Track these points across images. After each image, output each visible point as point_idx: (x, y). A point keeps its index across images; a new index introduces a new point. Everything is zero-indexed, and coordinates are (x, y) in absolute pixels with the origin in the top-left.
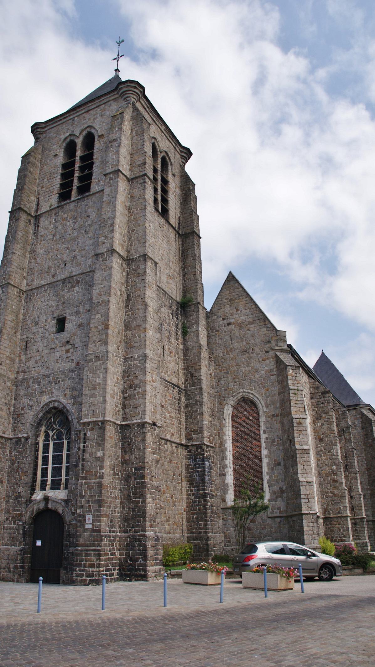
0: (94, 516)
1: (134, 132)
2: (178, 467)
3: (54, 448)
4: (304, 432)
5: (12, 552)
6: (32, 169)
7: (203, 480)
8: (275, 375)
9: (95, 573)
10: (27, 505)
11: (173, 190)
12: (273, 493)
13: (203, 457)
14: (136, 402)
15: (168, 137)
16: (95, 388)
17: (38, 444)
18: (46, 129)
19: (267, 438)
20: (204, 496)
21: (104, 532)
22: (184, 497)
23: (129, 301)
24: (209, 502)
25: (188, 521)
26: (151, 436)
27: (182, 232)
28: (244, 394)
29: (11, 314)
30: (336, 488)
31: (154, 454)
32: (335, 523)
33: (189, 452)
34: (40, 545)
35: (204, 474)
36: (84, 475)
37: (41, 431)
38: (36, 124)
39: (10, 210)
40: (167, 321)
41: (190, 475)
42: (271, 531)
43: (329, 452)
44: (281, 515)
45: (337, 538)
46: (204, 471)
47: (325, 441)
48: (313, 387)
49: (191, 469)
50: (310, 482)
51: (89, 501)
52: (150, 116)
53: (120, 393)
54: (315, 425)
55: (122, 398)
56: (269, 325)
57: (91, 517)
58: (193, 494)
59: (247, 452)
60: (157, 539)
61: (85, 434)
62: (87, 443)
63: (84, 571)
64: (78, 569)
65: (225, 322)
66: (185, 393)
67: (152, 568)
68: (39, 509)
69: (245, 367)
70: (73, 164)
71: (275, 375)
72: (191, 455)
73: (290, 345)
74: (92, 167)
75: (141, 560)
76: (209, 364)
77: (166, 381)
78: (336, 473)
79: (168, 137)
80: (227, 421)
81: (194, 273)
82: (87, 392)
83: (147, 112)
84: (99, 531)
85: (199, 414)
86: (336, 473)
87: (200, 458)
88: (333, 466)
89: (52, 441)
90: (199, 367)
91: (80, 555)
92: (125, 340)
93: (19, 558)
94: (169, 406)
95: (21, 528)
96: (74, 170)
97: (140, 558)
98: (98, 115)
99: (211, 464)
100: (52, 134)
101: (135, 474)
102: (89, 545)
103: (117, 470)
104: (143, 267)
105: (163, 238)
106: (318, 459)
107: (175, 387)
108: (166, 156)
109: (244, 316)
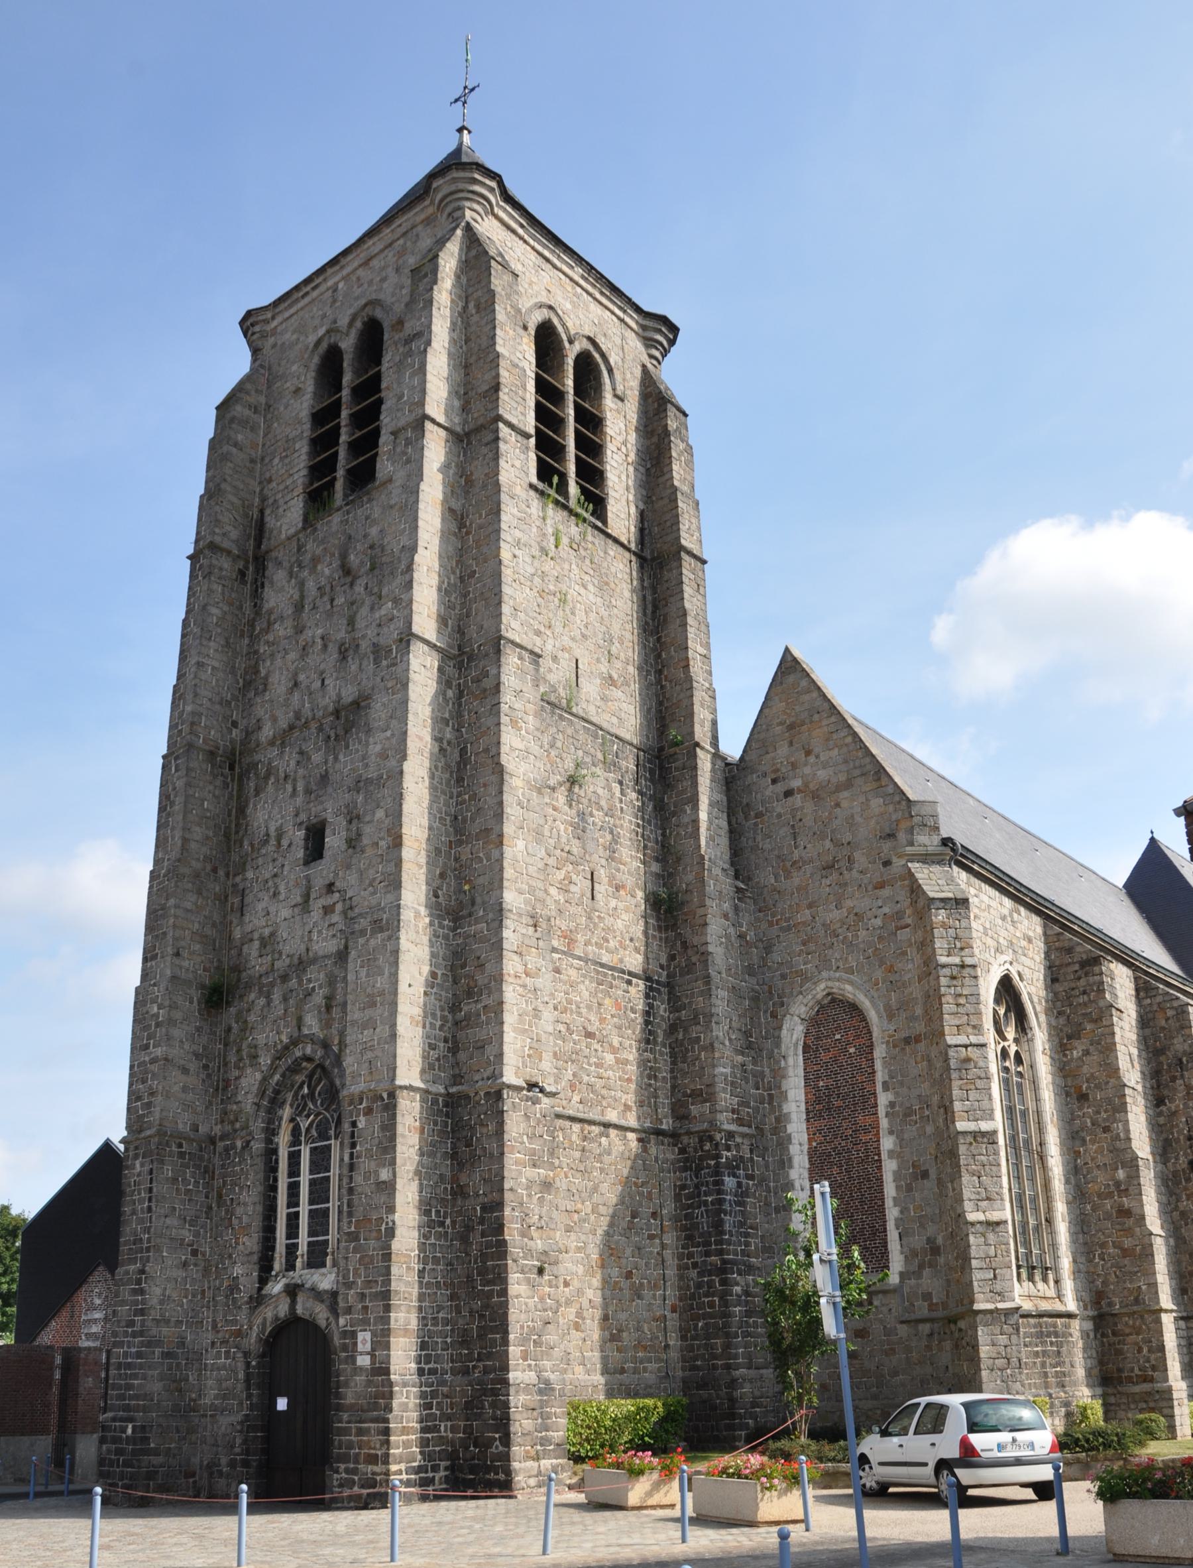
0: (374, 1335)
1: (471, 305)
2: (650, 1193)
3: (312, 1162)
4: (979, 1083)
5: (223, 1428)
6: (240, 437)
7: (718, 1225)
8: (907, 926)
9: (378, 1478)
10: (253, 1310)
11: (620, 439)
12: (910, 1255)
13: (718, 1165)
14: (481, 1034)
15: (598, 296)
16: (373, 1004)
17: (275, 1151)
18: (275, 323)
19: (892, 1105)
20: (723, 1270)
21: (400, 1375)
22: (671, 1272)
23: (465, 766)
24: (737, 1284)
25: (683, 1338)
26: (521, 1119)
27: (652, 552)
28: (830, 984)
29: (199, 825)
30: (1128, 1232)
31: (534, 1166)
32: (1127, 1331)
33: (682, 1151)
34: (285, 1408)
35: (720, 1211)
36: (353, 1229)
37: (281, 1118)
38: (249, 314)
39: (191, 551)
40: (603, 803)
41: (686, 1215)
42: (907, 1358)
43: (1106, 1129)
44: (934, 1315)
45: (1132, 1370)
46: (720, 1202)
47: (1095, 1099)
48: (1057, 949)
49: (688, 1197)
50: (998, 1224)
51: (363, 1296)
52: (533, 248)
53: (442, 1010)
54: (1064, 1055)
55: (449, 1025)
56: (890, 789)
57: (367, 1336)
58: (695, 1265)
59: (843, 1144)
60: (545, 1388)
61: (354, 1124)
62: (358, 1148)
63: (355, 1471)
64: (342, 1466)
65: (780, 788)
66: (669, 993)
67: (523, 1468)
68: (277, 1318)
69: (832, 911)
70: (333, 410)
71: (907, 926)
72: (686, 1160)
73: (950, 839)
74: (379, 412)
75: (498, 1443)
76: (736, 909)
77: (603, 965)
78: (1127, 1190)
79: (598, 296)
80: (791, 1061)
81: (682, 664)
82: (356, 1016)
83: (521, 238)
84: (387, 1372)
85: (704, 1048)
86: (1127, 1190)
87: (709, 1166)
88: (1117, 1169)
89: (306, 1144)
90: (701, 921)
91: (346, 1432)
92: (455, 870)
93: (238, 1441)
94: (615, 1031)
95: (241, 1365)
96: (338, 426)
97: (495, 1439)
98: (390, 269)
99: (744, 1181)
100: (287, 336)
101: (482, 1221)
102: (366, 1407)
103: (438, 1212)
104: (493, 671)
105: (587, 578)
106: (1075, 1152)
107: (634, 980)
108: (591, 349)
109: (824, 768)
